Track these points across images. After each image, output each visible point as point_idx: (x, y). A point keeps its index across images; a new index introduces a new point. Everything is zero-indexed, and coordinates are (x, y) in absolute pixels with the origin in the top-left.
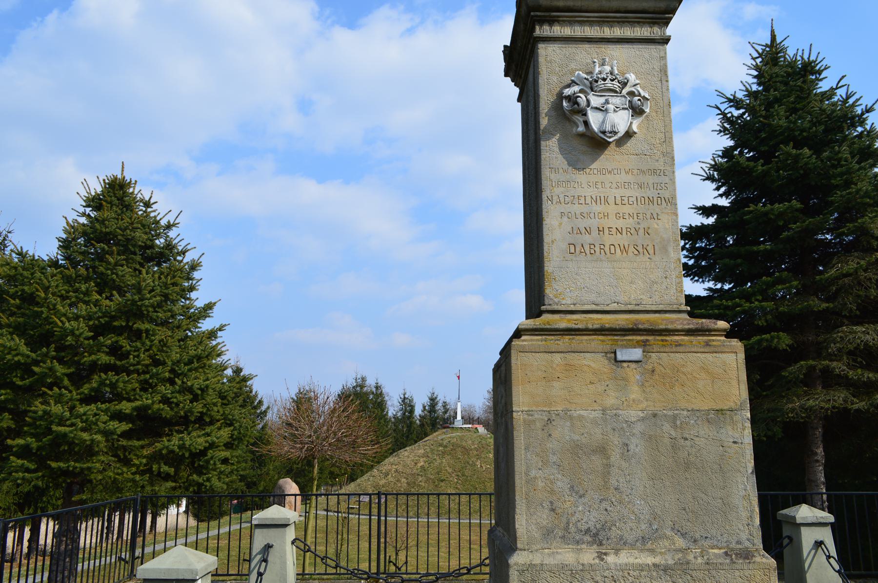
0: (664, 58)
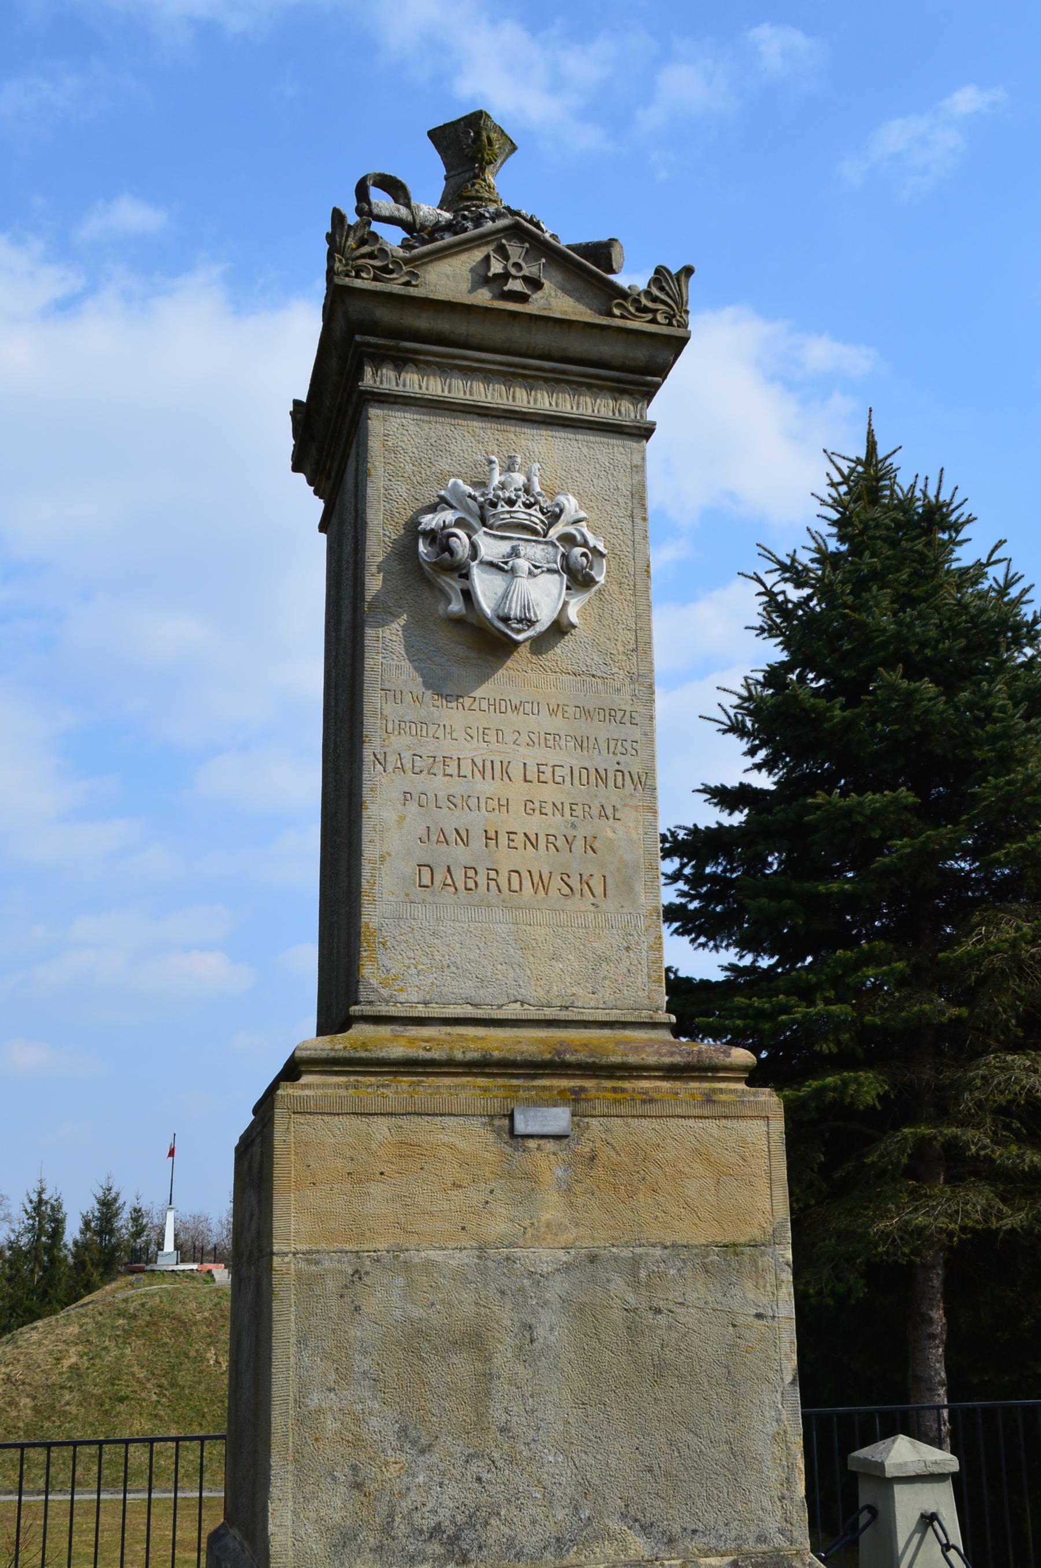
0: (639, 468)
